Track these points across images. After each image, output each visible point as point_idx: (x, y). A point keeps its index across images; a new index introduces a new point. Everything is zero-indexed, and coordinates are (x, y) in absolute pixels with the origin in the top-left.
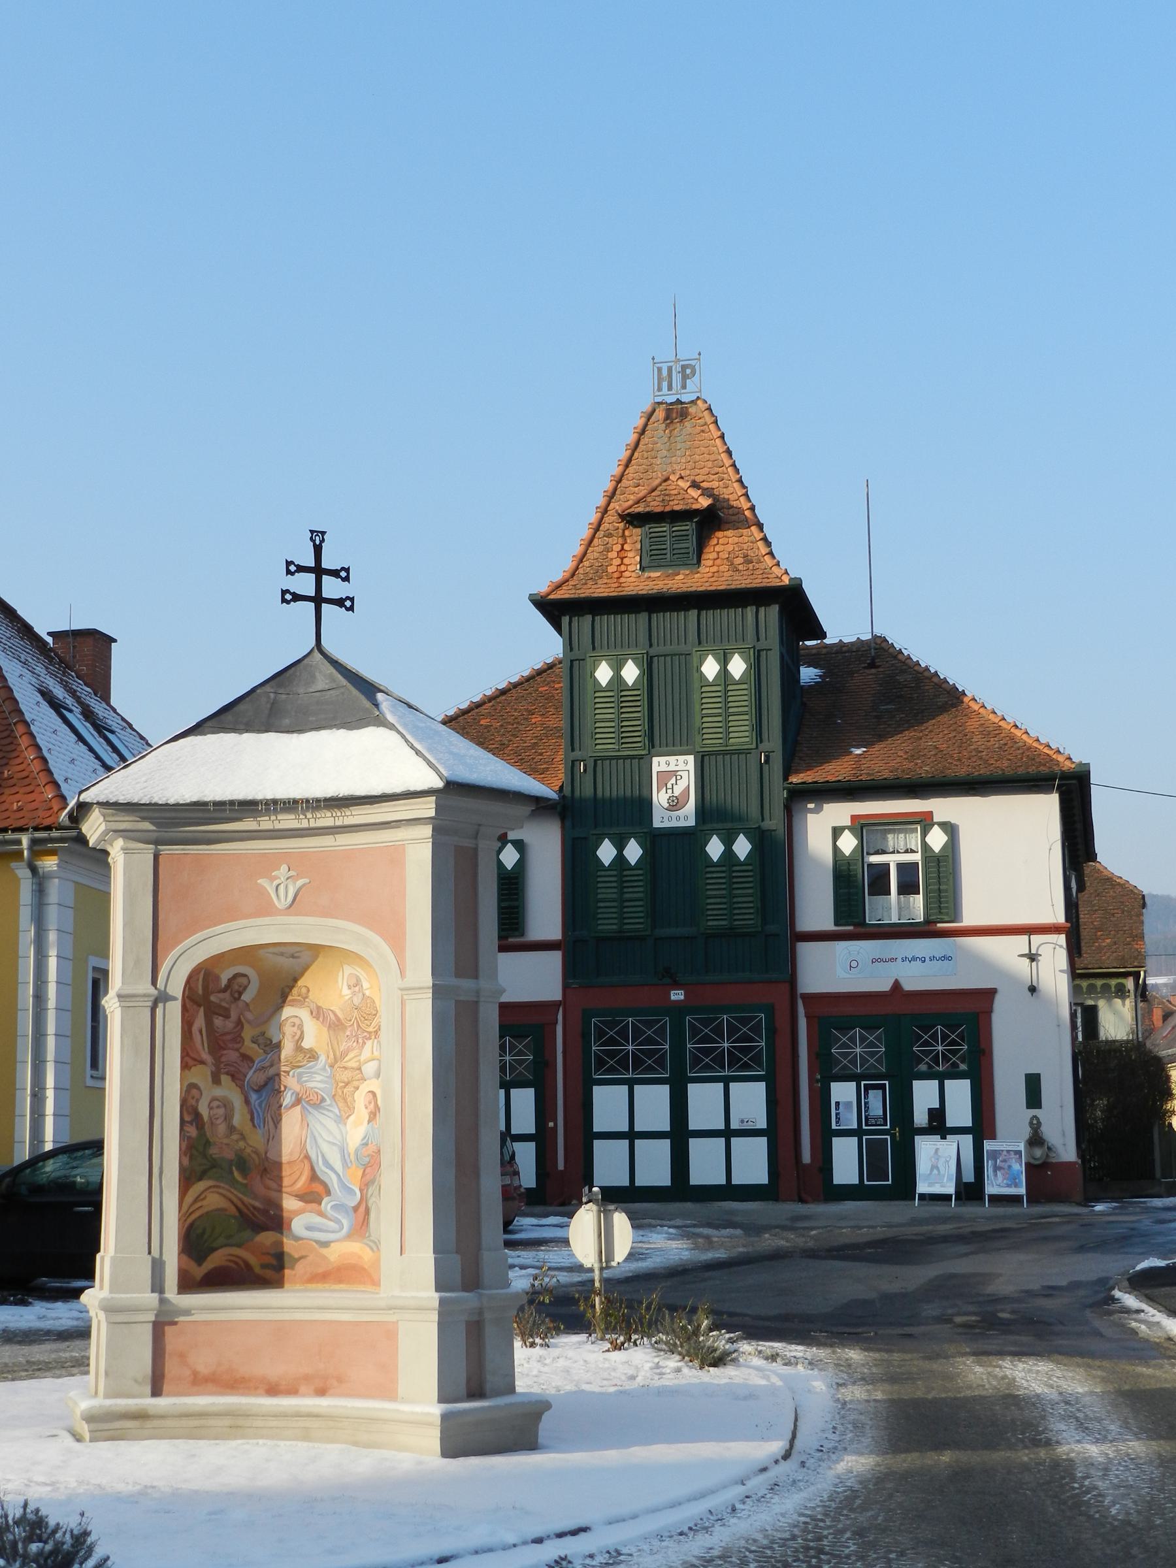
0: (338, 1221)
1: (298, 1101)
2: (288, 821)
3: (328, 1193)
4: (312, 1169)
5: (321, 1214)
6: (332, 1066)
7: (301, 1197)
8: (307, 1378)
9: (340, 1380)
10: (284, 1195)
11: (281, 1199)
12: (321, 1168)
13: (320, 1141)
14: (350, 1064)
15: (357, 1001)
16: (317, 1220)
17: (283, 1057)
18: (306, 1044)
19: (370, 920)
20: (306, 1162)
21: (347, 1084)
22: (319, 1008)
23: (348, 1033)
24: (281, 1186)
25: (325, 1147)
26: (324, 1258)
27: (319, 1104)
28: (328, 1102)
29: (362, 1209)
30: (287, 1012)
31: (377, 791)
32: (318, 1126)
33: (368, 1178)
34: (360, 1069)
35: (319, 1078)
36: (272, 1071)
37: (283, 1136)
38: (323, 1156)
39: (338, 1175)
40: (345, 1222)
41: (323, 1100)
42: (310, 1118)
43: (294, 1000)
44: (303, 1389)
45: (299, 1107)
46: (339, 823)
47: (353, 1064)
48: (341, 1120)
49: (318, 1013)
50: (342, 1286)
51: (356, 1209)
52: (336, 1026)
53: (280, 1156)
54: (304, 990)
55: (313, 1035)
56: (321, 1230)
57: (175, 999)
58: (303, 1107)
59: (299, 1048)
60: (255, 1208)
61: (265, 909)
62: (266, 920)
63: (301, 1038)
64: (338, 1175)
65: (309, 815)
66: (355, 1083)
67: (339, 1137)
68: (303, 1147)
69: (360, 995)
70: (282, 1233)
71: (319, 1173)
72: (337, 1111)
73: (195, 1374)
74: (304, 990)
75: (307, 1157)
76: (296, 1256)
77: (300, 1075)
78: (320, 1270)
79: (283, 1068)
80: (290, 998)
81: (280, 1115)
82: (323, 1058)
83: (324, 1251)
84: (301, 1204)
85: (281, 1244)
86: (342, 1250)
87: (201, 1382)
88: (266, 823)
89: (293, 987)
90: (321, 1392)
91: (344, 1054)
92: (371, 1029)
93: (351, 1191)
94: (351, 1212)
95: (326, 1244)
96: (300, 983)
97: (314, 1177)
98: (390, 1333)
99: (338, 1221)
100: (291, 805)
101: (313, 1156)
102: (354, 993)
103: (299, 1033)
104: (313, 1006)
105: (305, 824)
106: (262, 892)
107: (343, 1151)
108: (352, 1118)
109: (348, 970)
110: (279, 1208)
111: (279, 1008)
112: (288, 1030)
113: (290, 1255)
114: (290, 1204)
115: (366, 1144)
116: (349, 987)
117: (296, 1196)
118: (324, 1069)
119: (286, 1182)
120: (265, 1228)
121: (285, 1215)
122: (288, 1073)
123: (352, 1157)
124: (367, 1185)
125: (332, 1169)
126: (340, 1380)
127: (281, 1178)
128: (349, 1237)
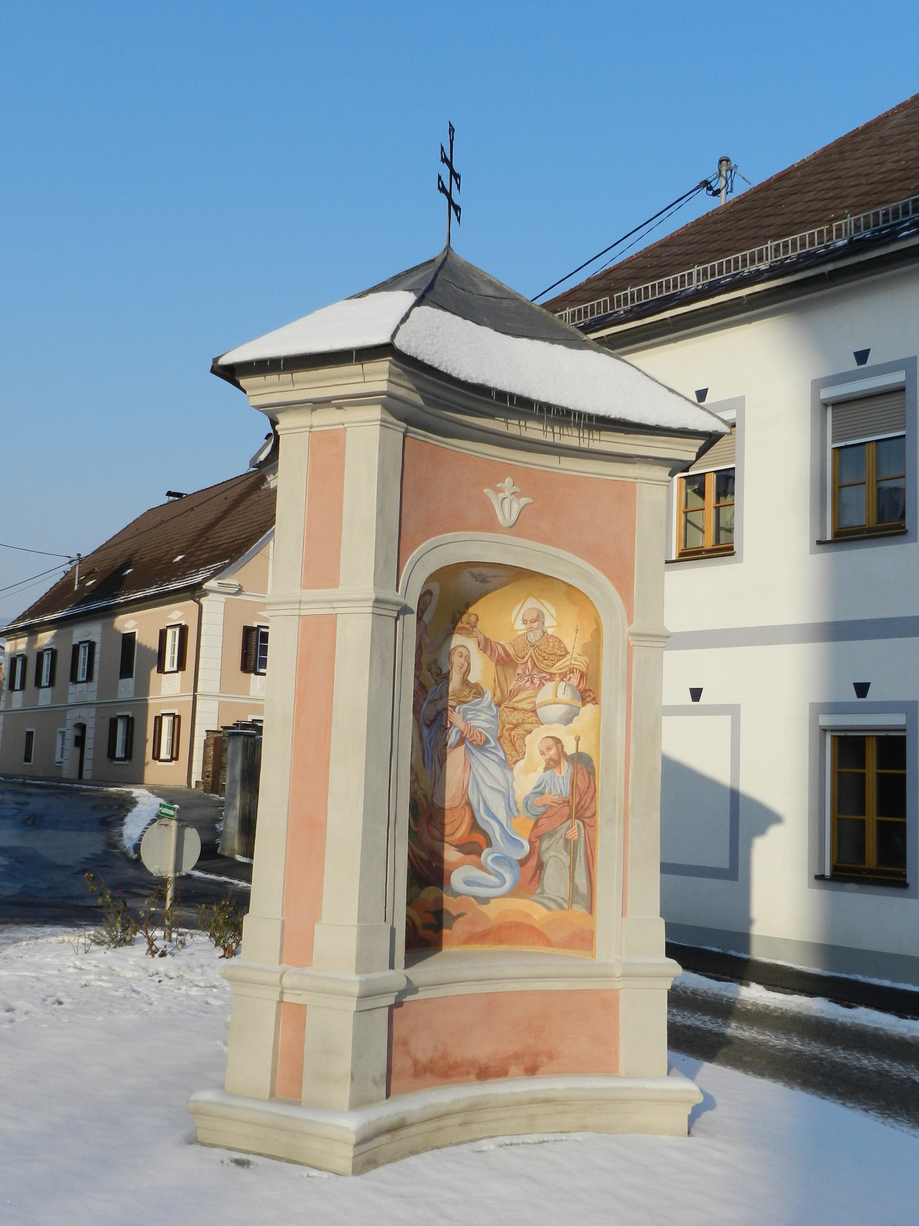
0: (499, 875)
1: (462, 741)
2: (534, 431)
3: (489, 844)
4: (473, 817)
5: (481, 867)
6: (498, 705)
7: (460, 847)
8: (517, 1057)
9: (550, 1056)
10: (446, 845)
11: (443, 848)
12: (482, 815)
13: (482, 786)
14: (519, 705)
15: (532, 637)
16: (477, 873)
17: (450, 690)
18: (473, 678)
19: (593, 554)
20: (467, 808)
21: (516, 726)
22: (487, 640)
23: (519, 671)
24: (443, 835)
25: (487, 793)
26: (483, 915)
27: (482, 746)
28: (493, 744)
29: (532, 863)
30: (457, 640)
31: (651, 421)
32: (481, 770)
33: (541, 830)
34: (534, 711)
35: (483, 716)
36: (440, 705)
37: (448, 778)
38: (485, 802)
39: (501, 825)
40: (509, 878)
41: (487, 741)
42: (473, 760)
43: (463, 628)
44: (513, 1069)
45: (462, 748)
46: (584, 445)
47: (525, 705)
48: (507, 764)
49: (486, 645)
50: (504, 947)
51: (522, 863)
52: (505, 662)
53: (444, 802)
54: (473, 618)
55: (480, 669)
56: (480, 885)
57: (412, 612)
58: (467, 748)
59: (465, 682)
60: (421, 859)
61: (489, 524)
62: (490, 536)
63: (468, 670)
64: (501, 825)
65: (557, 430)
66: (527, 727)
67: (503, 782)
68: (465, 793)
69: (539, 632)
70: (442, 888)
71: (480, 822)
72: (502, 754)
73: (416, 1063)
74: (473, 618)
75: (468, 803)
76: (454, 914)
77: (465, 712)
78: (478, 929)
79: (451, 703)
80: (460, 625)
81: (445, 755)
82: (488, 696)
83: (484, 908)
84: (460, 855)
85: (440, 900)
86: (503, 908)
87: (443, 1070)
88: (514, 428)
89: (464, 613)
90: (532, 1071)
91: (513, 694)
92: (553, 670)
93: (517, 843)
94: (517, 868)
95: (485, 900)
96: (471, 610)
97: (475, 826)
98: (607, 1003)
99: (499, 875)
100: (563, 416)
101: (474, 802)
102: (530, 630)
103: (466, 665)
104: (481, 637)
105: (549, 438)
106: (488, 507)
107: (507, 796)
108: (521, 764)
109: (532, 603)
110: (440, 859)
111: (449, 635)
112: (457, 660)
113: (449, 914)
114: (451, 855)
115: (541, 793)
116: (525, 622)
117: (456, 846)
118: (490, 707)
119: (448, 830)
120: (429, 884)
121: (446, 867)
122: (454, 707)
123: (520, 805)
124: (540, 837)
125: (494, 817)
126: (550, 1056)
127: (443, 825)
128: (511, 894)
